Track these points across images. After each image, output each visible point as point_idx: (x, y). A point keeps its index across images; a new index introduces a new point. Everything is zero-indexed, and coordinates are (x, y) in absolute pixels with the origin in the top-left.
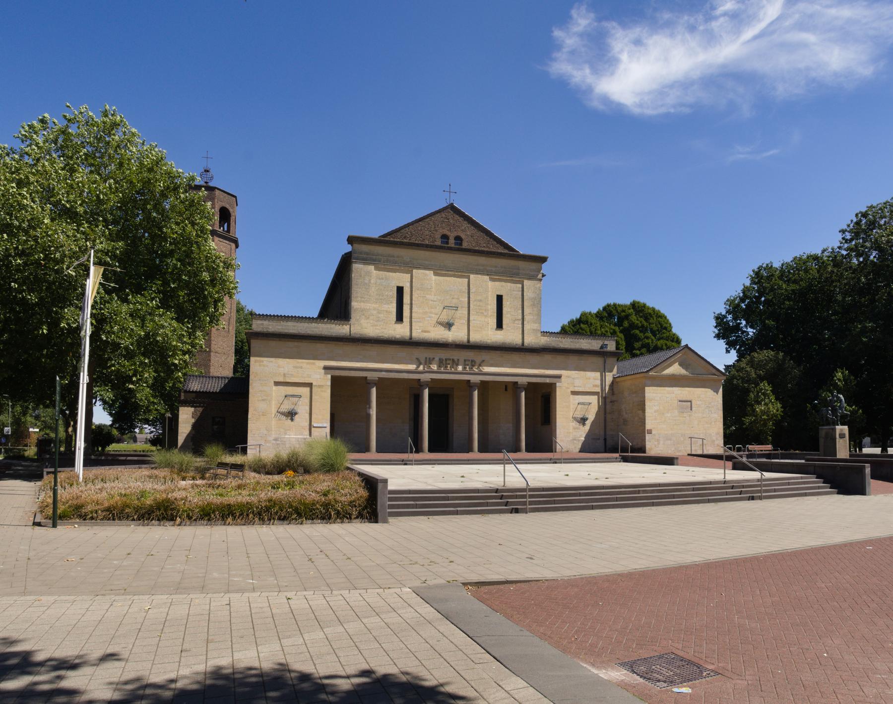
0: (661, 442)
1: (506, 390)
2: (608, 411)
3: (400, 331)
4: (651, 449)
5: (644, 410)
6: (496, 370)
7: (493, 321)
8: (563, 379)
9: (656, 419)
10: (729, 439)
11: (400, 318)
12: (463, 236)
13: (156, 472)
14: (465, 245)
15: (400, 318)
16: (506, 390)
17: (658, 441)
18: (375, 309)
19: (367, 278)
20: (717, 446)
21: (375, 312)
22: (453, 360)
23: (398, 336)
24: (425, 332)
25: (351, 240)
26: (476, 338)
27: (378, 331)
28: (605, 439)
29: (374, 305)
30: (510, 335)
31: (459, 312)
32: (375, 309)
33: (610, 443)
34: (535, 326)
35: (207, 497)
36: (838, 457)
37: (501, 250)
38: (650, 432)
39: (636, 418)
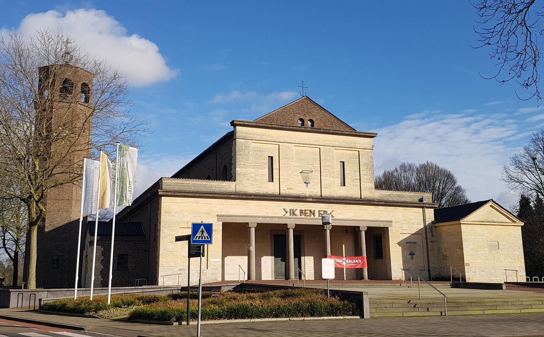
0: (477, 274)
2: (429, 249)
3: (272, 188)
4: (469, 279)
5: (462, 249)
7: (339, 181)
8: (394, 224)
9: (472, 255)
10: (529, 273)
11: (271, 179)
13: (252, 294)
14: (316, 126)
15: (271, 179)
17: (475, 272)
18: (253, 173)
19: (247, 151)
20: (522, 278)
21: (253, 175)
22: (310, 211)
23: (270, 193)
24: (290, 189)
25: (233, 124)
26: (326, 193)
27: (255, 189)
28: (429, 271)
29: (252, 170)
31: (314, 173)
32: (253, 173)
33: (433, 273)
35: (159, 308)
36: (433, 210)
37: (342, 129)
38: (468, 265)
39: (455, 255)
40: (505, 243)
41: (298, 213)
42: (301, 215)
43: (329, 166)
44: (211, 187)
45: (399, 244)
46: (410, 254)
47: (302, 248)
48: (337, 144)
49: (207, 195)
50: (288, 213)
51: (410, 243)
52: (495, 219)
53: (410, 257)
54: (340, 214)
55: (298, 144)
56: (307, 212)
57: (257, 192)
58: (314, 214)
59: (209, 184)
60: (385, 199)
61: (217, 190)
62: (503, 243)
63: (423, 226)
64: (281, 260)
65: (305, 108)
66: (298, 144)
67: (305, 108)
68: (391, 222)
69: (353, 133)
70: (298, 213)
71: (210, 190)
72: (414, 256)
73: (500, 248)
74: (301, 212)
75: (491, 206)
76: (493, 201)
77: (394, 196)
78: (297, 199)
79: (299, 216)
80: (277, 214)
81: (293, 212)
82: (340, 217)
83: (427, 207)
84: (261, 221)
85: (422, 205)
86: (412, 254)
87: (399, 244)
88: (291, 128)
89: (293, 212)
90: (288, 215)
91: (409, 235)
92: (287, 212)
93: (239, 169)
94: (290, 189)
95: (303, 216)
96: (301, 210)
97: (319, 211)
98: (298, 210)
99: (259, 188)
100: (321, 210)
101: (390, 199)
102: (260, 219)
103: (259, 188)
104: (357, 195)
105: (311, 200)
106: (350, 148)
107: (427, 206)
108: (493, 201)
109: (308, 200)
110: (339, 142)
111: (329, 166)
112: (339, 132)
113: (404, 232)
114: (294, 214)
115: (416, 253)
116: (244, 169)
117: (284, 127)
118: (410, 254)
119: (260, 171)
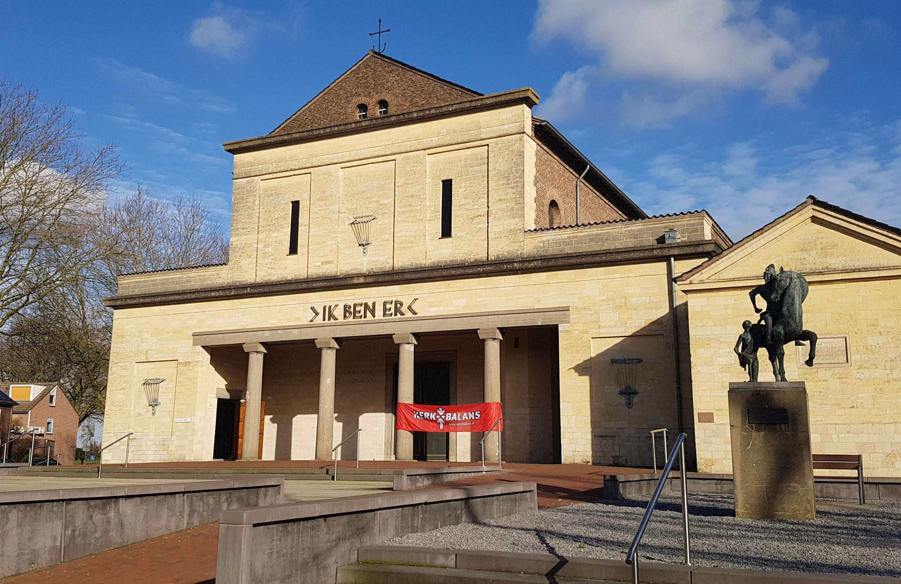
1: (517, 345)
6: (443, 306)
7: (437, 226)
8: (572, 315)
12: (388, 98)
16: (517, 345)
23: (289, 277)
24: (327, 263)
30: (465, 246)
31: (380, 221)
34: (514, 223)
37: (443, 98)
40: (882, 340)
41: (339, 313)
42: (345, 317)
43: (412, 196)
44: (188, 281)
45: (582, 369)
46: (622, 393)
47: (452, 388)
48: (435, 141)
49: (173, 298)
50: (321, 316)
51: (624, 361)
52: (835, 262)
53: (623, 400)
54: (432, 304)
55: (347, 164)
56: (358, 309)
57: (266, 278)
58: (373, 313)
59: (208, 273)
60: (552, 251)
61: (196, 285)
62: (871, 341)
63: (667, 311)
64: (271, 419)
65: (370, 80)
66: (347, 164)
67: (370, 80)
68: (566, 309)
69: (479, 103)
70: (339, 313)
71: (186, 288)
72: (636, 399)
73: (854, 357)
74: (346, 309)
75: (814, 219)
76: (816, 202)
77: (580, 241)
78: (332, 283)
79: (341, 319)
80: (299, 319)
81: (329, 313)
82: (433, 311)
83: (678, 258)
84: (269, 337)
85: (666, 252)
86: (628, 393)
87: (582, 369)
88: (328, 130)
89: (329, 313)
90: (319, 320)
91: (620, 339)
92: (317, 314)
93: (236, 238)
94: (327, 263)
95: (351, 319)
96: (345, 306)
97: (385, 303)
98: (341, 306)
99: (270, 271)
100: (357, 302)
101: (569, 250)
102: (267, 333)
103: (270, 271)
104: (479, 254)
105: (362, 280)
106: (466, 144)
107: (676, 252)
108: (816, 202)
109: (356, 281)
110: (439, 134)
111: (412, 196)
112: (433, 111)
113: (604, 332)
114: (331, 316)
115: (639, 388)
116: (243, 237)
117: (315, 133)
118: (622, 393)
119: (275, 234)
